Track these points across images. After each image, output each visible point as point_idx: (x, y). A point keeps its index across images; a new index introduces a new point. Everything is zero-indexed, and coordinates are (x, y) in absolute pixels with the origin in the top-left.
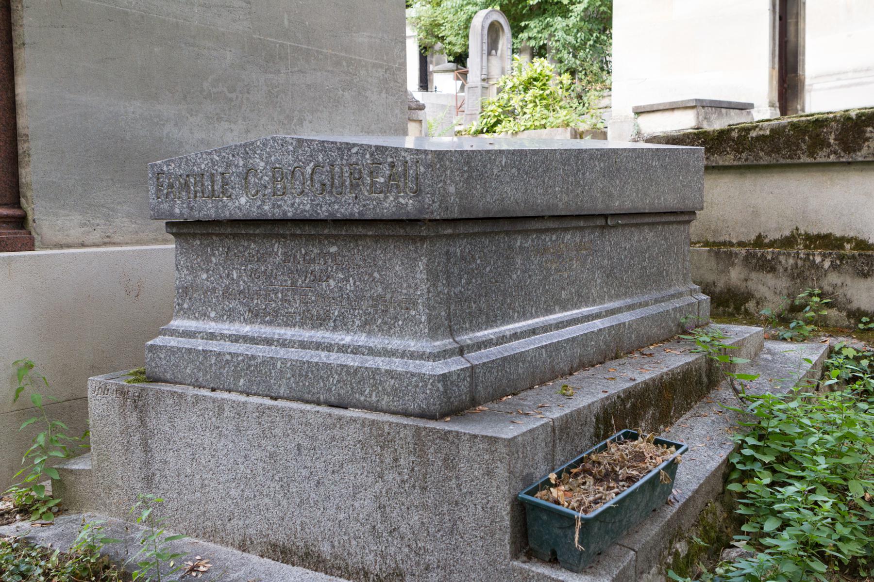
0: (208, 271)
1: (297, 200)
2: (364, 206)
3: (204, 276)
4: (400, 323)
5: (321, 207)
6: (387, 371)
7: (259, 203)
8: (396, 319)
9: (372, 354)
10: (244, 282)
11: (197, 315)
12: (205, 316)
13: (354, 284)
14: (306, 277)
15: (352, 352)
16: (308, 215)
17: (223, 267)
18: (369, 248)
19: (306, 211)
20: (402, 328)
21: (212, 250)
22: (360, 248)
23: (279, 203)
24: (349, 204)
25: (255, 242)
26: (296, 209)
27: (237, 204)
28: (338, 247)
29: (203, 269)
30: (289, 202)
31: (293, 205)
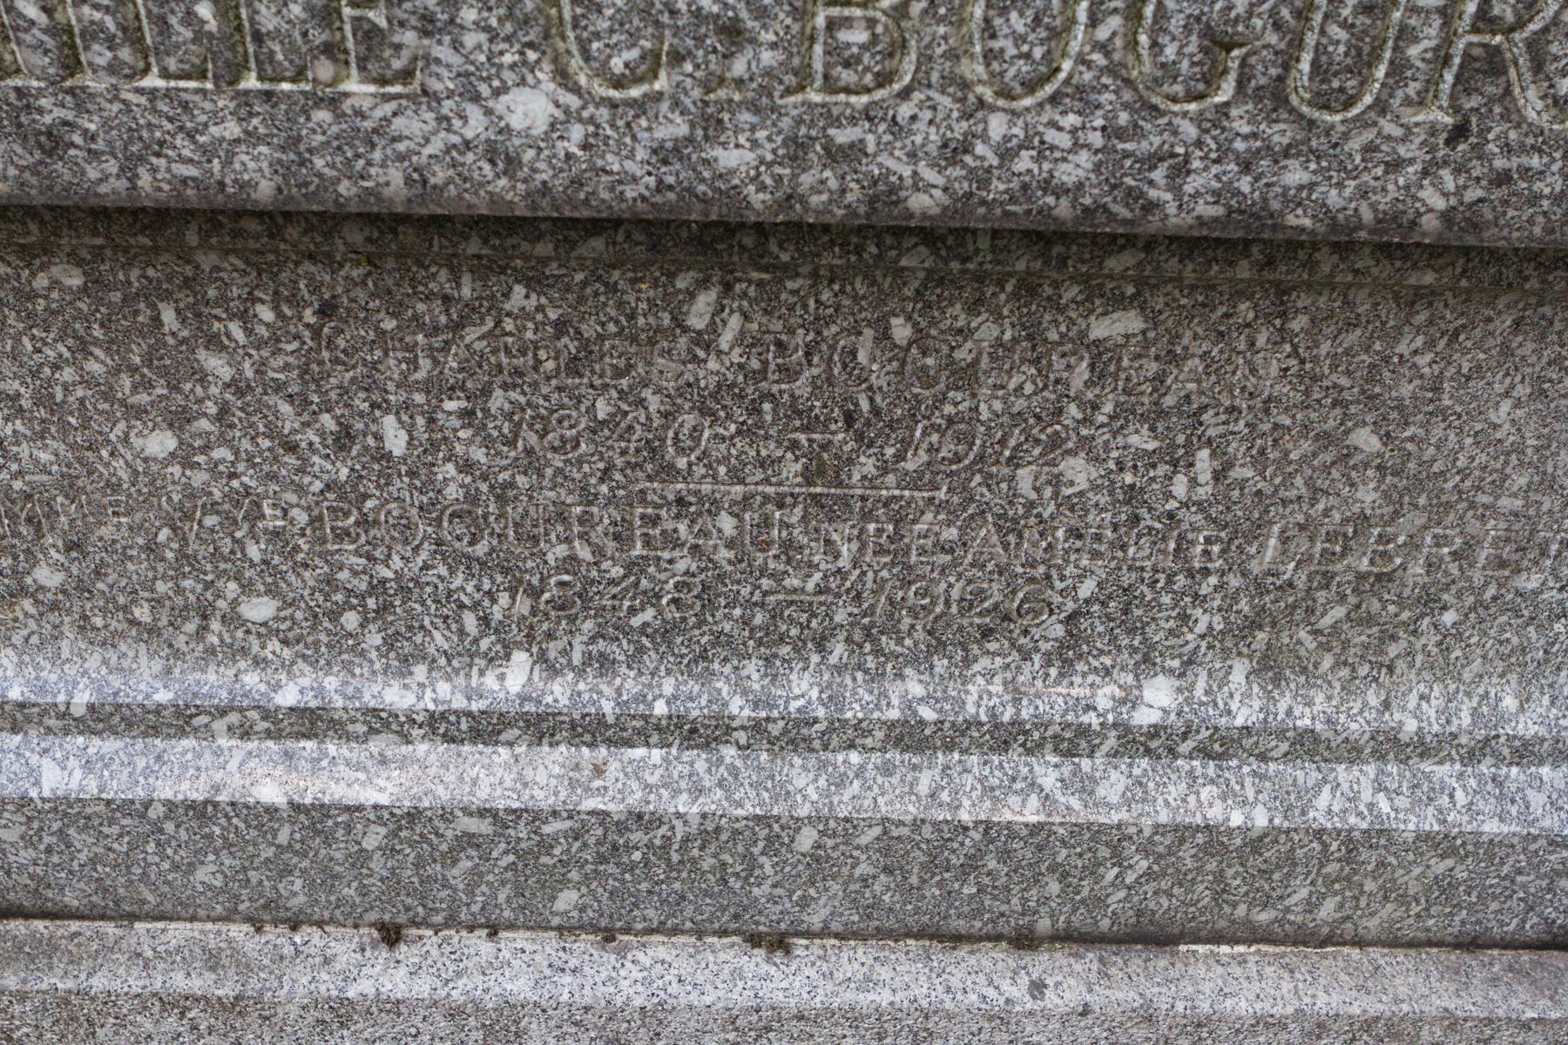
0: (178, 420)
1: (997, 126)
2: (1503, 178)
3: (160, 443)
4: (1449, 618)
5: (1181, 170)
6: (1423, 837)
7: (675, 128)
8: (1429, 602)
9: (1312, 755)
10: (467, 466)
11: (142, 613)
12: (407, 821)
13: (1218, 476)
14: (906, 443)
15: (1204, 752)
16: (1063, 209)
17: (300, 402)
18: (1351, 325)
19: (1060, 191)
20: (1447, 639)
21: (195, 314)
22: (1298, 323)
23: (842, 136)
24: (1395, 165)
25: (534, 283)
26: (982, 177)
27: (476, 125)
28: (1153, 319)
29: (139, 412)
30: (927, 135)
31: (953, 152)
